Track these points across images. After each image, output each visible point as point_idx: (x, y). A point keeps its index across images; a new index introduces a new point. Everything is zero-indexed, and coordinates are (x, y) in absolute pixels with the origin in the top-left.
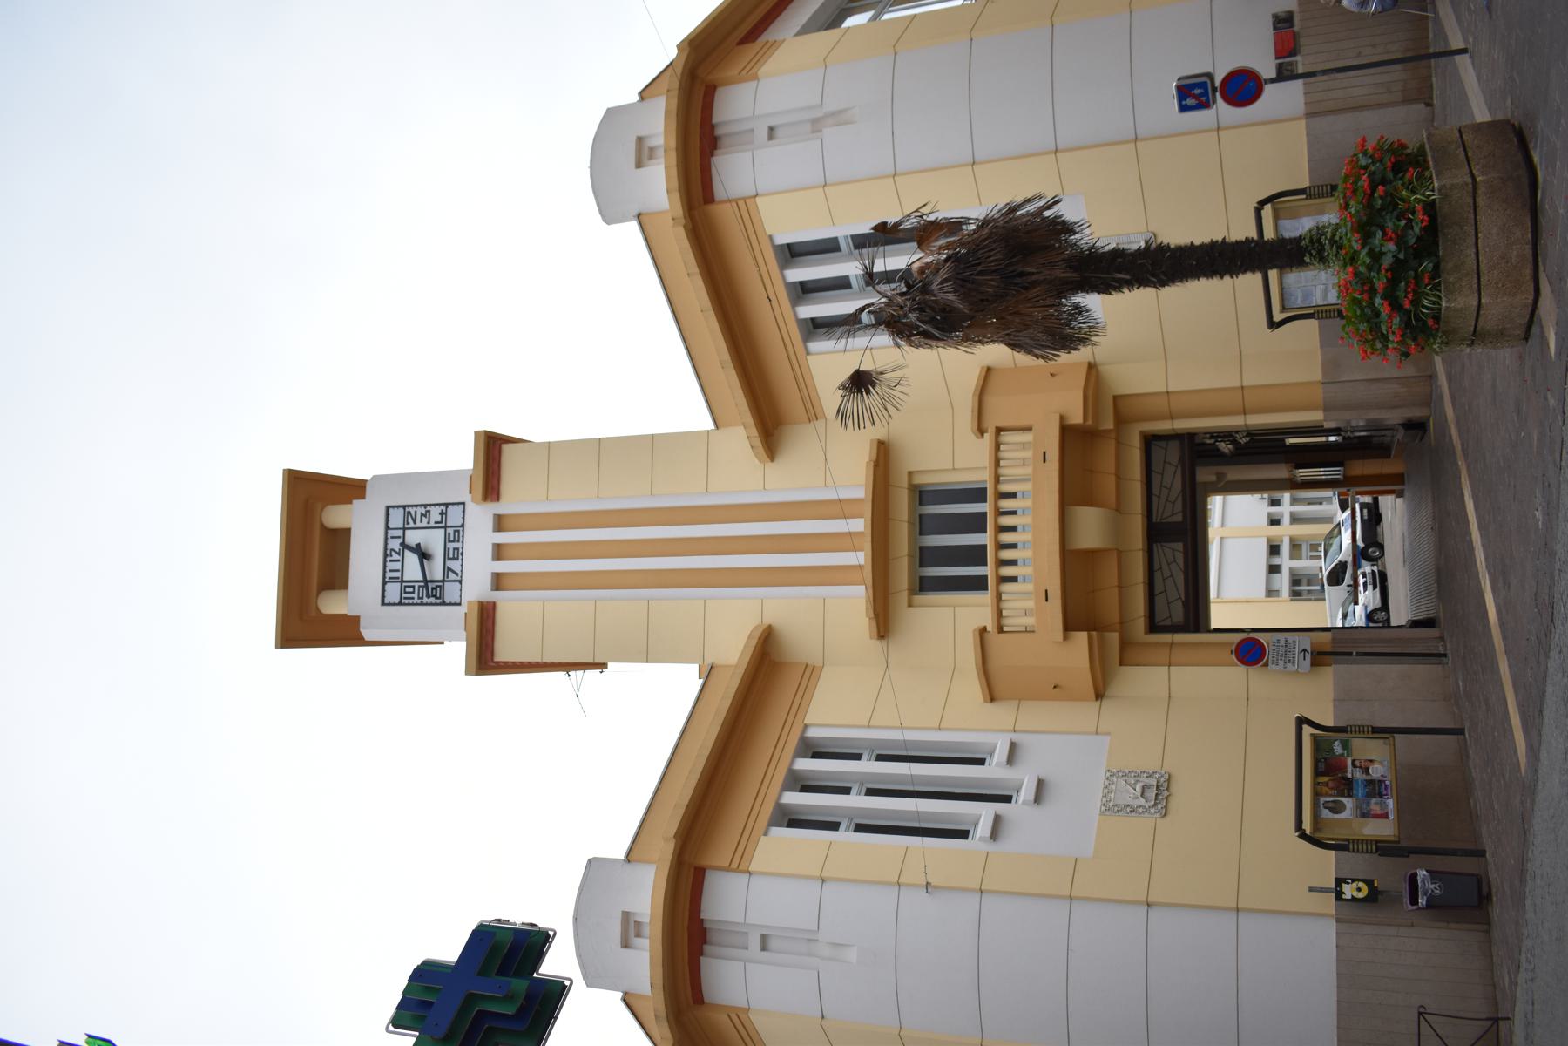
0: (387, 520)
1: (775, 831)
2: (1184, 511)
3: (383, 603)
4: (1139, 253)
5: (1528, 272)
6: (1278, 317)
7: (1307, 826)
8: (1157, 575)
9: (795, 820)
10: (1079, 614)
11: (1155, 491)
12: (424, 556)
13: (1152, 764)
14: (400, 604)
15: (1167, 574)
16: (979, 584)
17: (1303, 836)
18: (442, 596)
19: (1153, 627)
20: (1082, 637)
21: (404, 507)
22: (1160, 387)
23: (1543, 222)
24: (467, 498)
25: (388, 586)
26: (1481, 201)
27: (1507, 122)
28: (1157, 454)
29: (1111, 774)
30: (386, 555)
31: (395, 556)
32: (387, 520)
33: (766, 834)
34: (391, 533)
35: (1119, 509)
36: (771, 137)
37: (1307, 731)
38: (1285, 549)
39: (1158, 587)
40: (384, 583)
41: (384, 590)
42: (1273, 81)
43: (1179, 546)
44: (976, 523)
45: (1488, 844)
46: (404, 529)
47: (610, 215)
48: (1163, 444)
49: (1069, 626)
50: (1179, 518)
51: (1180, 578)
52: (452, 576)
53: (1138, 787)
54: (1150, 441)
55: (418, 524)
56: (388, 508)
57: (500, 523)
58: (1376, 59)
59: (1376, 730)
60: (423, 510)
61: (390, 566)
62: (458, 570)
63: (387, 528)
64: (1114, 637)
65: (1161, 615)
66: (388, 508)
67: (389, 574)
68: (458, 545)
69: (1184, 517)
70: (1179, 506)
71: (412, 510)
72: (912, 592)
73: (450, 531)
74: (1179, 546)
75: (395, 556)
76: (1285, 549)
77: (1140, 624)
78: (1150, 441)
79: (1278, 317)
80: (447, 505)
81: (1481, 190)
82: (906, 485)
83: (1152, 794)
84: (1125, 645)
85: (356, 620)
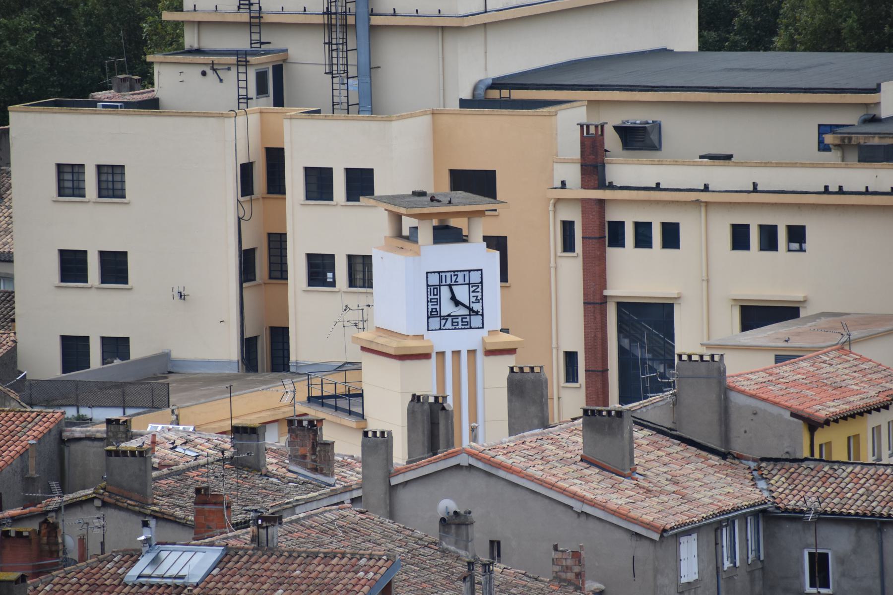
21: (481, 283)
31: (454, 278)
46: (469, 284)
55: (472, 295)
56: (427, 273)
60: (479, 298)
61: (448, 275)
66: (427, 273)
67: (443, 274)
75: (454, 278)
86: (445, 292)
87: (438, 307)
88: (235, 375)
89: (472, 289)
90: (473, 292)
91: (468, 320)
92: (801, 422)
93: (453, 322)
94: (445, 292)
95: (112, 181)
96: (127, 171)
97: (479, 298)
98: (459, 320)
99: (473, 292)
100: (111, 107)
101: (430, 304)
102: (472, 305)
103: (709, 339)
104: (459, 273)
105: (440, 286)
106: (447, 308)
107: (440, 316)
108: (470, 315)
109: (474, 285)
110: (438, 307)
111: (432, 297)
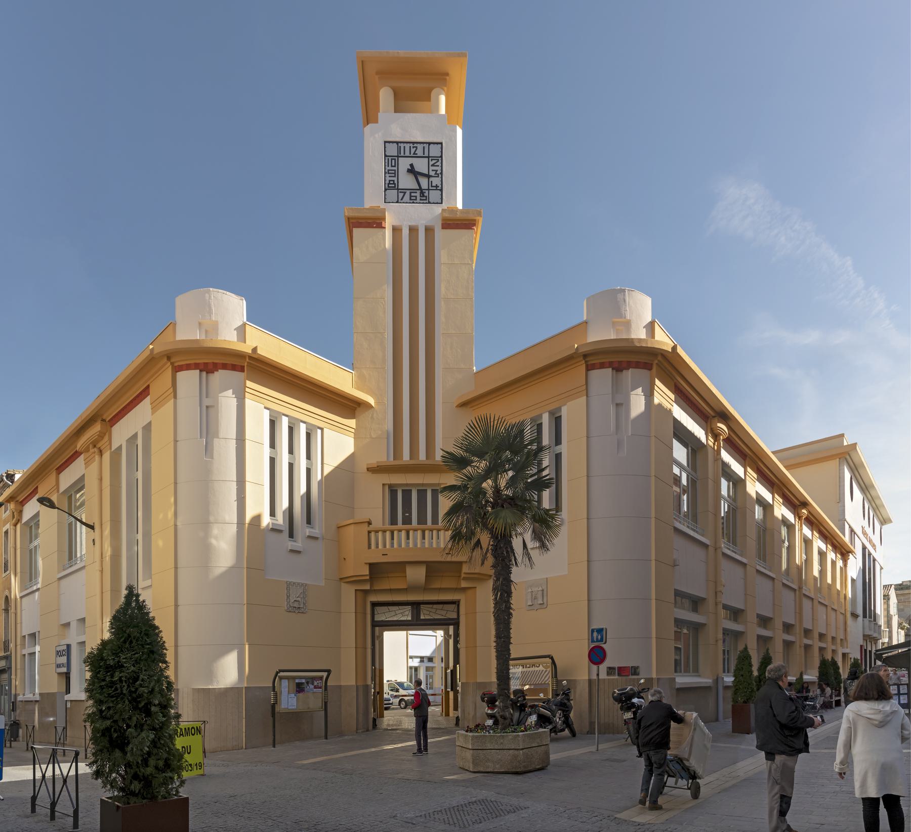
0: (434, 143)
1: (267, 413)
3: (385, 142)
5: (482, 769)
7: (282, 674)
9: (273, 423)
10: (376, 570)
11: (435, 606)
12: (412, 170)
14: (386, 156)
16: (393, 521)
17: (277, 673)
22: (235, 483)
23: (501, 776)
24: (445, 205)
26: (511, 752)
27: (548, 764)
29: (304, 586)
30: (413, 143)
31: (413, 150)
33: (265, 408)
34: (426, 146)
35: (426, 589)
37: (325, 674)
38: (430, 664)
40: (397, 143)
41: (393, 142)
42: (244, 325)
43: (410, 618)
44: (422, 520)
45: (278, 747)
49: (372, 566)
51: (395, 619)
52: (401, 195)
53: (299, 599)
54: (456, 603)
55: (431, 168)
56: (441, 143)
57: (429, 230)
58: (271, 733)
59: (326, 703)
60: (439, 172)
61: (407, 146)
62: (404, 200)
63: (429, 144)
64: (367, 587)
65: (378, 609)
66: (441, 143)
67: (402, 145)
68: (418, 200)
69: (412, 617)
72: (390, 486)
74: (410, 618)
75: (413, 150)
76: (430, 664)
78: (456, 603)
80: (441, 190)
81: (516, 752)
83: (296, 605)
84: (366, 592)
85: (376, 121)
89: (431, 163)
90: (433, 165)
97: (439, 172)
99: (433, 165)
104: (418, 145)
110: (395, 179)
111: (390, 168)
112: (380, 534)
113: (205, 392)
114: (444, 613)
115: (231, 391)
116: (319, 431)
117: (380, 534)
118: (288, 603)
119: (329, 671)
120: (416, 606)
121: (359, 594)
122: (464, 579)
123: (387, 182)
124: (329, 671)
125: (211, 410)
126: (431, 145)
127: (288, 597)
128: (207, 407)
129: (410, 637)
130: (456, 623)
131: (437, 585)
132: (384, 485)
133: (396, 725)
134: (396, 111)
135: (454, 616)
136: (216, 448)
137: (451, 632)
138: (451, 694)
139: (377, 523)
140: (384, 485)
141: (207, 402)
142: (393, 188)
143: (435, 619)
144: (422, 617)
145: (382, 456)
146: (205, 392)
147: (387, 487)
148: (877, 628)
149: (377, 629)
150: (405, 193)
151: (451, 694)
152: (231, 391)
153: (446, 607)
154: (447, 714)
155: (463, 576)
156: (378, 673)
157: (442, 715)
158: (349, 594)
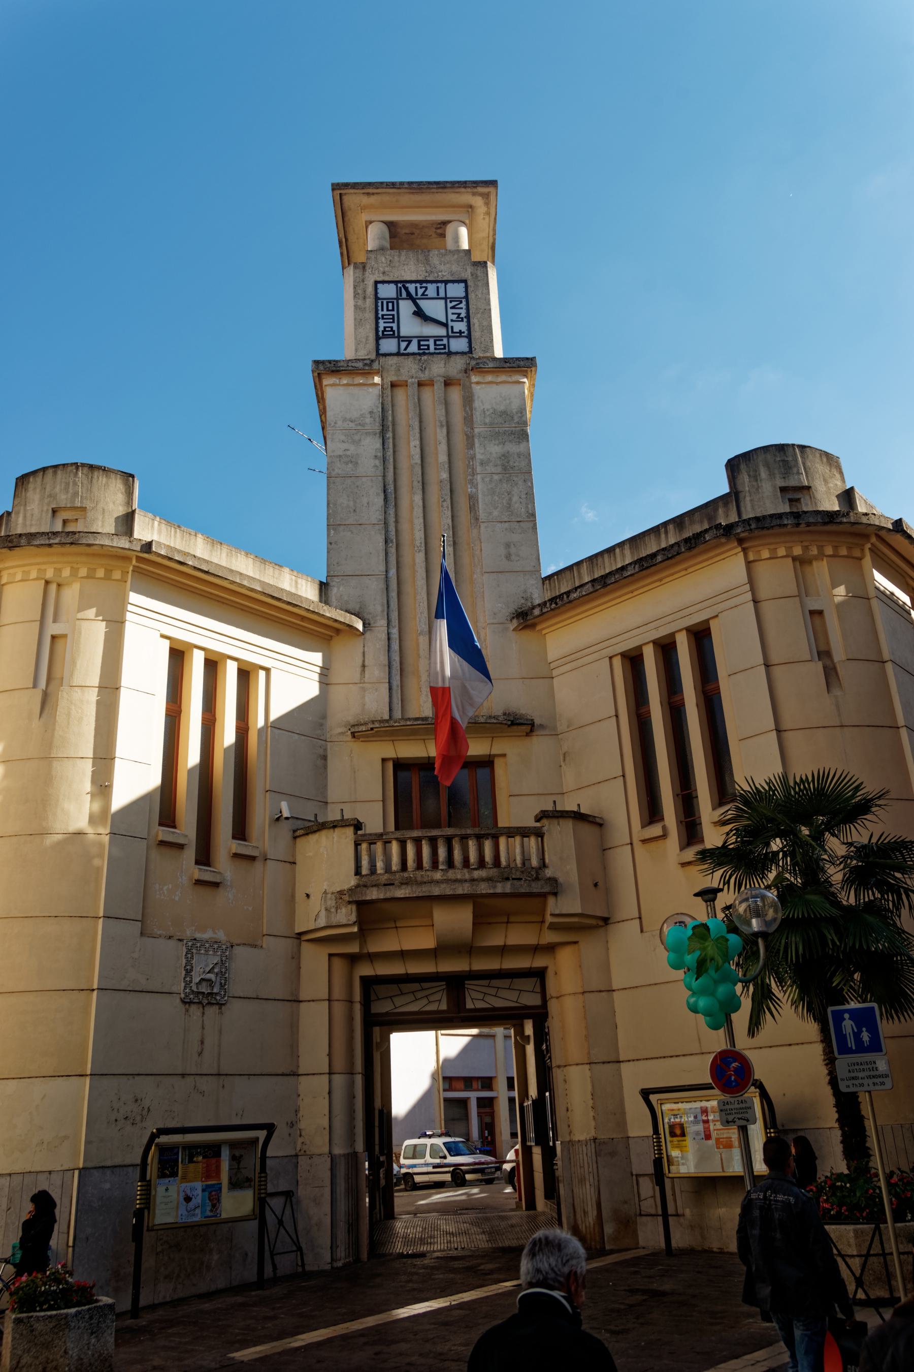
2: (476, 1010)
4: (37, 1208)
6: (653, 1098)
7: (164, 1139)
8: (416, 986)
11: (495, 983)
13: (235, 989)
15: (419, 995)
17: (153, 1137)
18: (385, 336)
19: (368, 983)
20: (346, 915)
21: (466, 297)
25: (393, 286)
28: (530, 983)
30: (421, 282)
31: (420, 291)
32: (453, 282)
33: (163, 636)
36: (812, 613)
37: (262, 1135)
39: (406, 987)
43: (444, 1006)
46: (446, 298)
47: (734, 466)
48: (538, 989)
50: (469, 1005)
52: (403, 345)
53: (211, 976)
54: (540, 974)
55: (450, 311)
56: (376, 283)
60: (463, 315)
63: (446, 282)
64: (354, 948)
65: (382, 990)
70: (480, 1005)
71: (463, 305)
73: (445, 341)
74: (444, 1006)
75: (420, 291)
77: (366, 970)
79: (653, 1098)
82: (494, 752)
83: (204, 989)
84: (353, 959)
86: (406, 307)
87: (395, 326)
88: (753, 1172)
89: (450, 305)
90: (453, 308)
91: (445, 341)
92: (427, 314)
93: (419, 345)
94: (406, 307)
95: (850, 1071)
96: (538, 361)
97: (463, 315)
98: (431, 343)
99: (453, 308)
100: (38, 546)
101: (381, 321)
102: (450, 324)
103: (438, 287)
104: (429, 285)
105: (397, 299)
106: (409, 326)
107: (399, 337)
108: (448, 337)
109: (399, 292)
110: (395, 326)
111: (385, 312)
112: (379, 846)
113: (48, 607)
114: (513, 996)
115: (94, 610)
116: (262, 674)
117: (379, 846)
118: (187, 984)
119: (270, 1128)
120: (455, 984)
121: (337, 962)
122: (553, 927)
123: (381, 329)
124: (270, 1128)
125: (60, 643)
126: (449, 286)
127: (188, 972)
128: (53, 637)
129: (441, 1038)
130: (540, 1016)
131: (496, 939)
132: (384, 760)
133: (422, 1241)
134: (333, 185)
135: (533, 1000)
136: (62, 704)
137: (529, 1030)
138: (537, 1153)
139: (374, 823)
140: (384, 760)
141: (53, 629)
142: (393, 336)
143: (494, 1009)
144: (469, 1005)
145: (375, 703)
146: (48, 607)
147: (390, 766)
148: (897, 540)
149: (377, 1030)
150: (410, 342)
151: (537, 1153)
152: (94, 610)
153: (519, 983)
154: (531, 1205)
155: (549, 919)
156: (81, 586)
157: (518, 1207)
158: (315, 961)
